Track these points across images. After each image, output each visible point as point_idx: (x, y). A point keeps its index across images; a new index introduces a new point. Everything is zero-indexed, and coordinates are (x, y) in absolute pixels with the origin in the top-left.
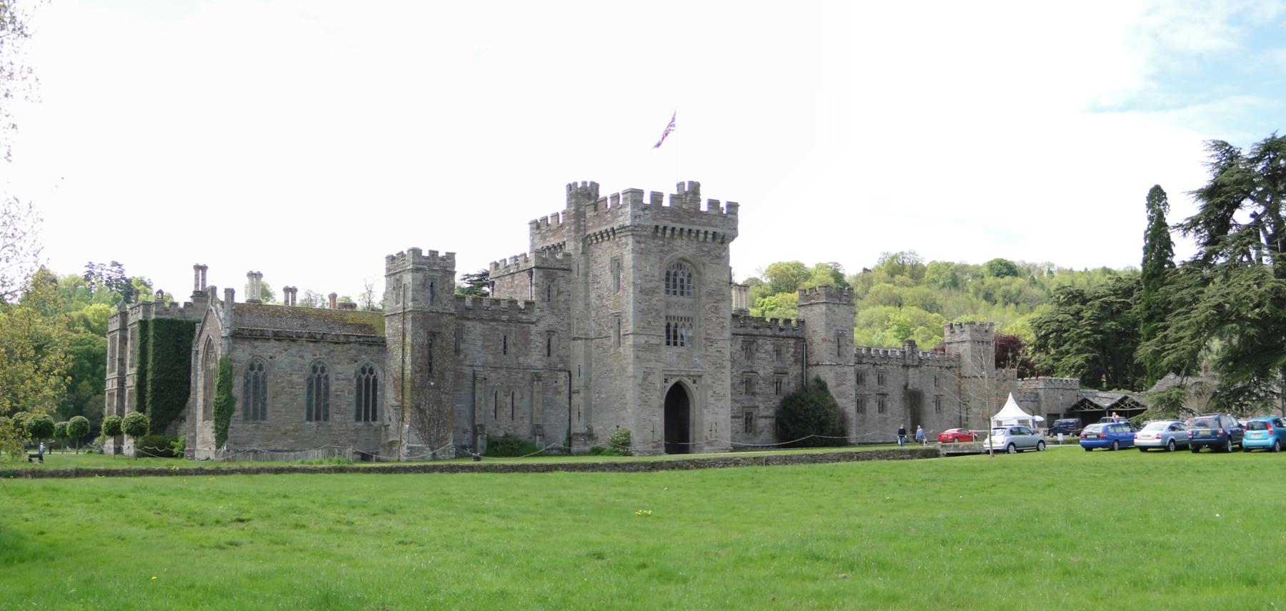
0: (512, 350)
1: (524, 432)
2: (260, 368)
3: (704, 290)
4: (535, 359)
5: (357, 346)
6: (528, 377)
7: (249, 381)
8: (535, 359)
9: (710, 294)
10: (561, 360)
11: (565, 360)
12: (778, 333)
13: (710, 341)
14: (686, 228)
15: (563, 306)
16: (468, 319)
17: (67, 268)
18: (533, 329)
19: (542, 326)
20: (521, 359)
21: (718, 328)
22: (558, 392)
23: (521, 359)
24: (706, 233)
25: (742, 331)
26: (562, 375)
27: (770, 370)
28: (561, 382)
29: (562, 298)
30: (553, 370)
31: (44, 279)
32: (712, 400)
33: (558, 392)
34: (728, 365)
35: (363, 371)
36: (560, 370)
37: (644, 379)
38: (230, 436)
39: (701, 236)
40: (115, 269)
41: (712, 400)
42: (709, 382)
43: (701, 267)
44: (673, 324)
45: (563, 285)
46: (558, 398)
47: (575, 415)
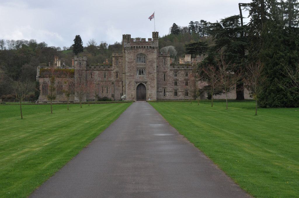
0: (106, 77)
1: (110, 96)
2: (46, 84)
3: (148, 61)
4: (113, 79)
5: (69, 78)
6: (111, 83)
7: (43, 86)
8: (113, 79)
9: (150, 62)
10: (120, 79)
11: (121, 79)
12: (186, 69)
13: (150, 73)
14: (144, 46)
15: (120, 66)
16: (95, 70)
17: (183, 24)
18: (112, 72)
19: (114, 71)
20: (109, 79)
21: (152, 70)
22: (119, 86)
23: (109, 79)
24: (147, 47)
25: (173, 69)
26: (121, 82)
27: (183, 79)
28: (120, 84)
29: (120, 64)
30: (118, 81)
31: (175, 29)
32: (150, 88)
33: (119, 86)
34: (156, 79)
35: (71, 83)
36: (120, 81)
37: (129, 83)
38: (39, 98)
39: (146, 48)
40: (203, 23)
41: (150, 88)
42: (149, 83)
43: (147, 55)
44: (141, 69)
45: (120, 61)
46: (119, 88)
47: (123, 92)
